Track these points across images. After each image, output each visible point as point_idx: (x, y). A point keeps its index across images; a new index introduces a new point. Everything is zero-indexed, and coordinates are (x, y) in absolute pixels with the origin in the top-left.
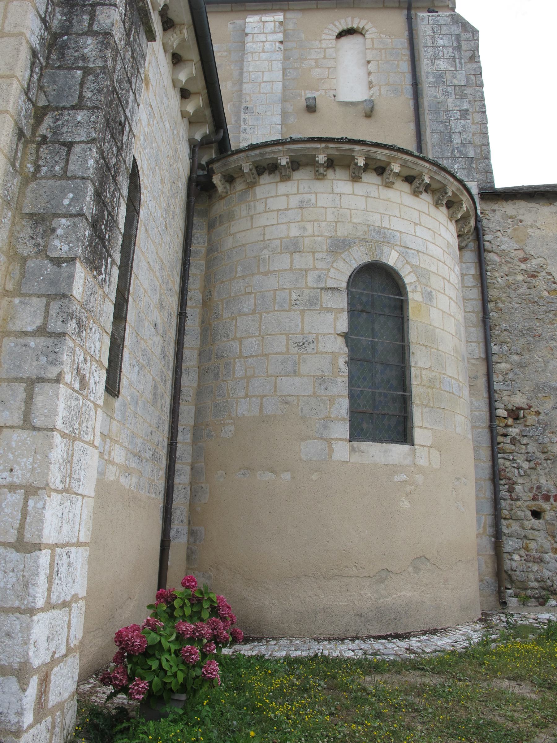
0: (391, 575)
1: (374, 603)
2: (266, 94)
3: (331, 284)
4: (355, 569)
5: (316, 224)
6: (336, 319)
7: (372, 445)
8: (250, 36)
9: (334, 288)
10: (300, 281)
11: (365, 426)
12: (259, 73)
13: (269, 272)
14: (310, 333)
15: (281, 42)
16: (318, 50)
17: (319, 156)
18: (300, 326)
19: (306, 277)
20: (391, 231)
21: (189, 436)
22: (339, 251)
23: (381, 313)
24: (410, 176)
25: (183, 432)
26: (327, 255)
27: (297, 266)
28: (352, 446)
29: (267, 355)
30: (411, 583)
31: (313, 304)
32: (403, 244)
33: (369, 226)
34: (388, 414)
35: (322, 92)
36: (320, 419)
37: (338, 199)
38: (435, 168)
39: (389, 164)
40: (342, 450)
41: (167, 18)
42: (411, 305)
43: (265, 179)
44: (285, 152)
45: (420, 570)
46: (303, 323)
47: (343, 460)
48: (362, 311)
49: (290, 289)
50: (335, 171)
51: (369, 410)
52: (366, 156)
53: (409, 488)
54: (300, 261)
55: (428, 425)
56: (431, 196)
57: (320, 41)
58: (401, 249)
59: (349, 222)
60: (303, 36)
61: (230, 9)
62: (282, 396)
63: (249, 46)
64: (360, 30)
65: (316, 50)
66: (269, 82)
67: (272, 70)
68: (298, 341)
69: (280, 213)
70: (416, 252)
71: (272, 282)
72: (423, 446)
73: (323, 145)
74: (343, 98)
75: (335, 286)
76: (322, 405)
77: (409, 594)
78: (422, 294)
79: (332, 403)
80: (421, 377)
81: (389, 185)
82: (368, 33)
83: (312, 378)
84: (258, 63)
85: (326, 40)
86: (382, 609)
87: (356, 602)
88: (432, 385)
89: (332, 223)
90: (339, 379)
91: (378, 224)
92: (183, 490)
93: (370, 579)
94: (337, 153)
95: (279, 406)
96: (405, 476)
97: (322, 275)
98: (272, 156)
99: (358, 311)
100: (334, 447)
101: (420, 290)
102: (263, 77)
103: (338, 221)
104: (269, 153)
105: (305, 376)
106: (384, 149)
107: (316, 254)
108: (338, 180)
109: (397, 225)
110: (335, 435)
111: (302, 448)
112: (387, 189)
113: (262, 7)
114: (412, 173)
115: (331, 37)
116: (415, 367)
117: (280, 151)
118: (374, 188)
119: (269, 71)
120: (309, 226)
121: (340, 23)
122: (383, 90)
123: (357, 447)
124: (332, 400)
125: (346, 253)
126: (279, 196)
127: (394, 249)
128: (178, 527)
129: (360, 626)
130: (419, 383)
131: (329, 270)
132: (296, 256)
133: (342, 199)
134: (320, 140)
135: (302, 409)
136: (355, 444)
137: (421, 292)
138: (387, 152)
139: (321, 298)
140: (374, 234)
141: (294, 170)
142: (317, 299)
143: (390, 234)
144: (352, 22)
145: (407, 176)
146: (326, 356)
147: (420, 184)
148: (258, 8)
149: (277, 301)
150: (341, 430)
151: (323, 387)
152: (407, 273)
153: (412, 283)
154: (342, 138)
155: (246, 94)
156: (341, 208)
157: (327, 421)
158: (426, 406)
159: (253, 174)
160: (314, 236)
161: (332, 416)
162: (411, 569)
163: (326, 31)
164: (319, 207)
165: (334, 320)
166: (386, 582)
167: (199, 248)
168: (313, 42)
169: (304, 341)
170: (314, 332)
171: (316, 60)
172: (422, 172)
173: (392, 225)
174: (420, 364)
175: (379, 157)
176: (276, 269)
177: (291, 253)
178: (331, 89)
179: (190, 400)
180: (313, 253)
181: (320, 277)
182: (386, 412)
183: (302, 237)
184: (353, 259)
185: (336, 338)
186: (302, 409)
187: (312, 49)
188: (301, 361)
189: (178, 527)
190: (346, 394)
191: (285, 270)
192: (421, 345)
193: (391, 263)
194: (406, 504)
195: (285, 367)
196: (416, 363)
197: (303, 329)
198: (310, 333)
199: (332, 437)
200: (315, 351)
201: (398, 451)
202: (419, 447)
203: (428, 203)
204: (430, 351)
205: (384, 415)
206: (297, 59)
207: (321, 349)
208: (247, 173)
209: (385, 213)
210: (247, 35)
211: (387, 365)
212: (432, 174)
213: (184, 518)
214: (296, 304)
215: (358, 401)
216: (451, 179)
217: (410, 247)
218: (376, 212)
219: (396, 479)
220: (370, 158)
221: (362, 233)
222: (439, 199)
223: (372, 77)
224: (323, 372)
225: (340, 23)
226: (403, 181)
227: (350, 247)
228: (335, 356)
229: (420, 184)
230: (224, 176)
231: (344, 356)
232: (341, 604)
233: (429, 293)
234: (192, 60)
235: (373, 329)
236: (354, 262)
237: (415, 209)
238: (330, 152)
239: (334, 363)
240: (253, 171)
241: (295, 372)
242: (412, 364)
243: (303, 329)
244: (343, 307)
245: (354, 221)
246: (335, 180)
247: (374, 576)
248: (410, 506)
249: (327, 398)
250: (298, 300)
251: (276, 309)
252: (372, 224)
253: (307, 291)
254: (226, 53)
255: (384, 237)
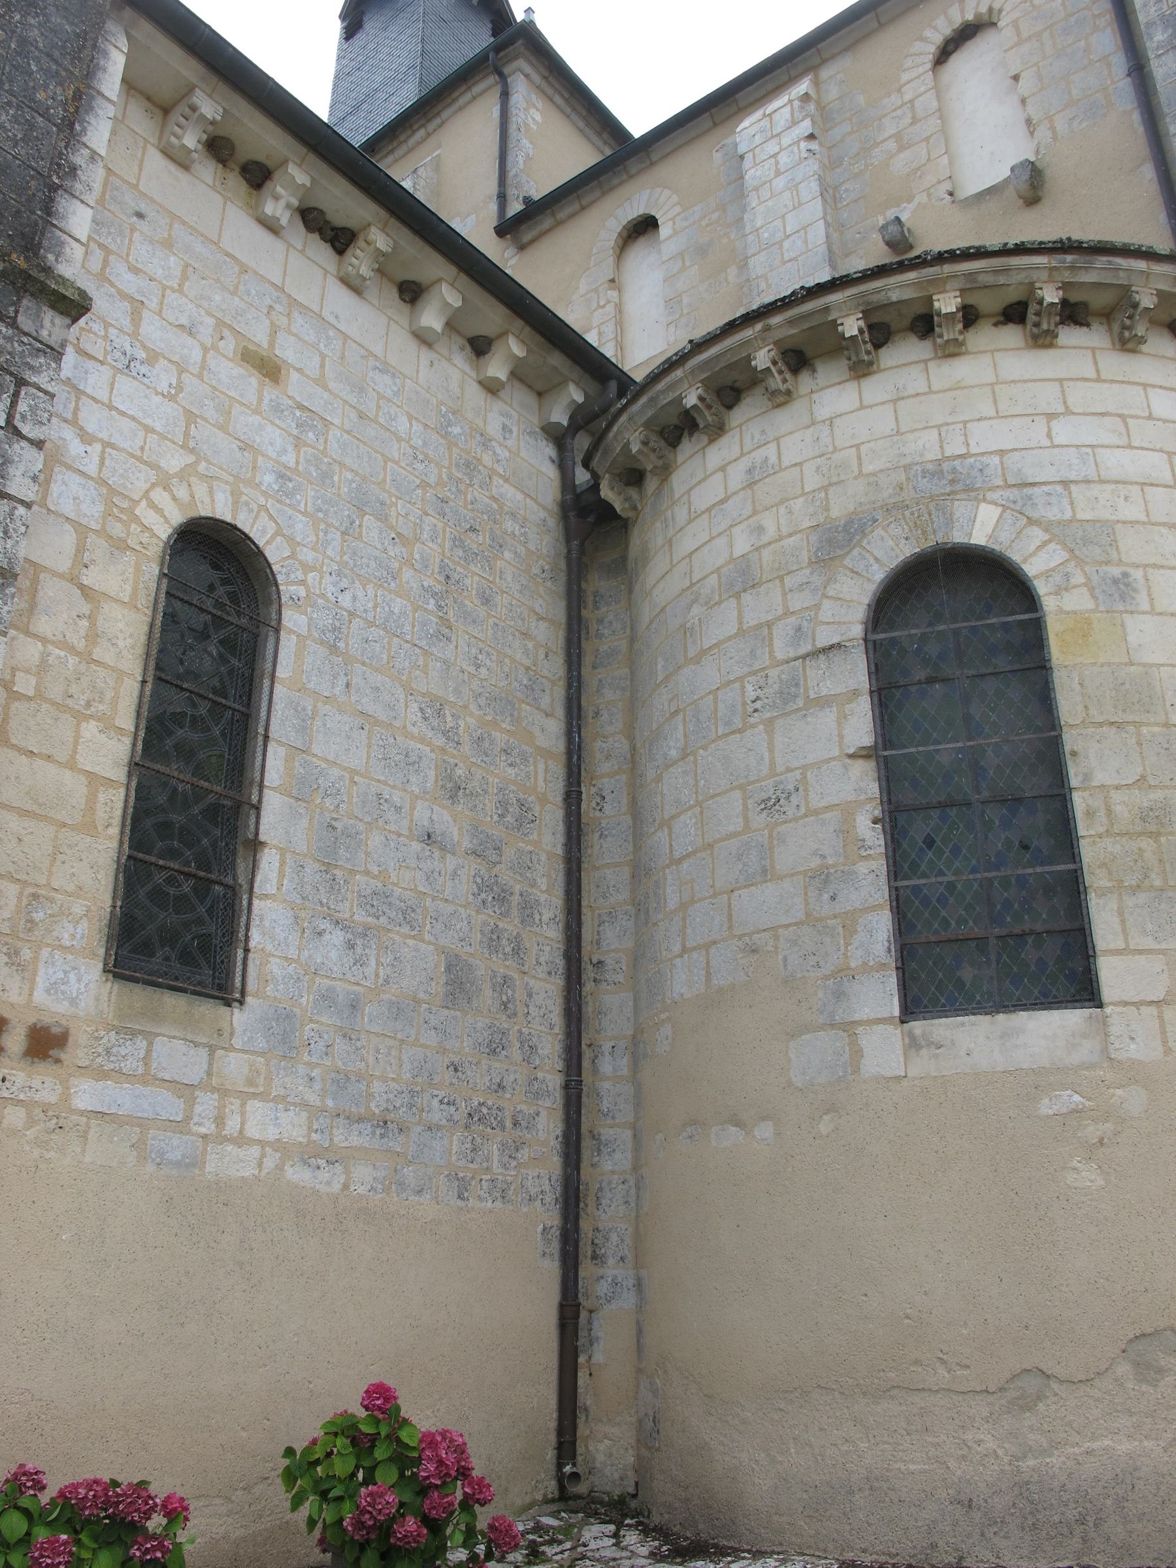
0: (1055, 1386)
1: (1007, 1468)
2: (795, 259)
3: (825, 637)
4: (942, 1371)
5: (782, 510)
6: (842, 718)
7: (963, 1024)
8: (749, 157)
9: (832, 647)
10: (759, 652)
11: (967, 974)
12: (776, 223)
13: (704, 652)
14: (789, 770)
15: (812, 137)
16: (899, 112)
17: (757, 354)
18: (767, 760)
19: (771, 640)
20: (972, 460)
21: (625, 1061)
22: (839, 552)
23: (984, 670)
24: (1011, 306)
25: (612, 1054)
26: (812, 573)
27: (751, 620)
28: (911, 1035)
29: (711, 846)
30: (1131, 1414)
31: (792, 699)
32: (1011, 481)
33: (907, 468)
34: (1032, 932)
35: (921, 198)
36: (826, 978)
37: (826, 430)
38: (1069, 258)
39: (929, 300)
40: (884, 1049)
41: (333, 229)
42: (1054, 628)
43: (687, 447)
44: (690, 378)
45: (1161, 1371)
46: (771, 750)
47: (888, 1074)
48: (931, 680)
49: (740, 679)
50: (814, 371)
51: (978, 932)
52: (861, 308)
53: (1092, 1132)
54: (758, 607)
55: (1149, 943)
56: (1103, 329)
57: (899, 91)
58: (1008, 493)
59: (855, 478)
60: (861, 99)
61: (711, 124)
62: (744, 935)
63: (752, 175)
64: (986, 17)
65: (894, 114)
66: (798, 231)
67: (800, 205)
68: (764, 796)
69: (713, 512)
70: (1059, 488)
71: (709, 674)
72: (1137, 1005)
73: (759, 327)
74: (972, 185)
75: (835, 640)
76: (828, 940)
77: (1124, 1447)
78: (1092, 590)
79: (850, 931)
80: (1109, 812)
81: (952, 349)
82: (1004, 13)
83: (801, 877)
84: (770, 203)
85: (912, 80)
86: (1032, 1487)
87: (952, 1464)
88: (1153, 828)
89: (816, 494)
90: (862, 868)
91: (933, 454)
92: (620, 1187)
93: (990, 1399)
94: (792, 331)
95: (741, 962)
96: (1077, 1098)
97: (805, 623)
98: (671, 396)
99: (919, 682)
100: (863, 1042)
101: (1082, 580)
102: (785, 227)
103: (830, 485)
104: (663, 392)
105: (786, 876)
106: (902, 272)
107: (787, 580)
108: (822, 389)
109: (987, 438)
110: (864, 1012)
111: (792, 1056)
112: (951, 361)
113: (770, 87)
114: (1012, 296)
115: (921, 70)
116: (1085, 789)
117: (681, 380)
118: (916, 372)
119: (794, 208)
120: (768, 521)
121: (935, 28)
122: (1061, 125)
123: (924, 1034)
124: (849, 923)
125: (855, 552)
126: (711, 475)
127: (984, 500)
128: (615, 1272)
129: (969, 1536)
130: (1102, 830)
131: (817, 607)
132: (747, 598)
133: (835, 428)
134: (749, 319)
135: (785, 959)
136: (918, 1026)
137: (1085, 585)
138: (912, 275)
139: (805, 680)
140: (923, 483)
141: (730, 407)
142: (797, 685)
143: (972, 467)
144: (962, 11)
145: (1005, 309)
146: (828, 816)
147: (1038, 314)
148: (763, 92)
149: (720, 714)
150: (880, 995)
151: (826, 897)
152: (1033, 548)
153: (1053, 570)
154: (793, 293)
155: (758, 277)
156: (835, 450)
157: (843, 978)
158: (1136, 889)
159: (654, 450)
160: (781, 538)
161: (853, 965)
162: (1123, 1369)
163: (909, 63)
164: (787, 468)
165: (839, 724)
166: (1041, 1406)
167: (616, 643)
168: (885, 101)
169: (778, 793)
170: (796, 764)
171: (898, 136)
172: (1032, 284)
173: (972, 443)
174: (1099, 778)
175: (895, 297)
176: (714, 642)
177: (737, 596)
178: (939, 182)
179: (622, 980)
180: (781, 578)
181: (799, 629)
182: (1027, 927)
183: (757, 549)
184: (872, 561)
185: (845, 767)
186: (785, 959)
187: (885, 115)
188: (775, 842)
189: (615, 1272)
190: (881, 901)
191: (730, 638)
192: (1101, 724)
193: (979, 538)
194: (1087, 1177)
195: (744, 865)
196: (1087, 777)
197: (772, 764)
198: (789, 770)
199: (857, 1017)
200: (803, 810)
201: (1046, 1032)
202: (1119, 1009)
203: (1093, 350)
204: (1139, 734)
205: (1022, 936)
206: (858, 154)
207: (816, 802)
208: (640, 451)
209: (949, 421)
210: (742, 157)
211: (1019, 800)
212: (1067, 276)
213: (626, 1252)
214: (756, 710)
215: (943, 913)
216: (1141, 265)
217: (1037, 480)
218: (926, 428)
219: (1046, 1107)
220: (876, 309)
221: (890, 491)
222: (1124, 328)
223: (1031, 110)
224: (823, 857)
225: (935, 28)
226: (995, 325)
227: (864, 535)
228: (848, 811)
229: (1038, 314)
230: (619, 475)
231: (868, 807)
232: (912, 1467)
233: (1115, 582)
234: (440, 280)
235: (967, 718)
236: (876, 567)
237: (1049, 380)
238: (779, 334)
239: (846, 830)
240: (652, 444)
241: (764, 871)
242: (1074, 782)
243: (772, 764)
244: (856, 687)
245: (868, 468)
246: (817, 391)
247: (1001, 1389)
248: (1101, 1182)
249: (839, 920)
250: (758, 698)
251: (720, 733)
252: (918, 459)
253: (773, 673)
254: (717, 214)
255: (956, 481)
